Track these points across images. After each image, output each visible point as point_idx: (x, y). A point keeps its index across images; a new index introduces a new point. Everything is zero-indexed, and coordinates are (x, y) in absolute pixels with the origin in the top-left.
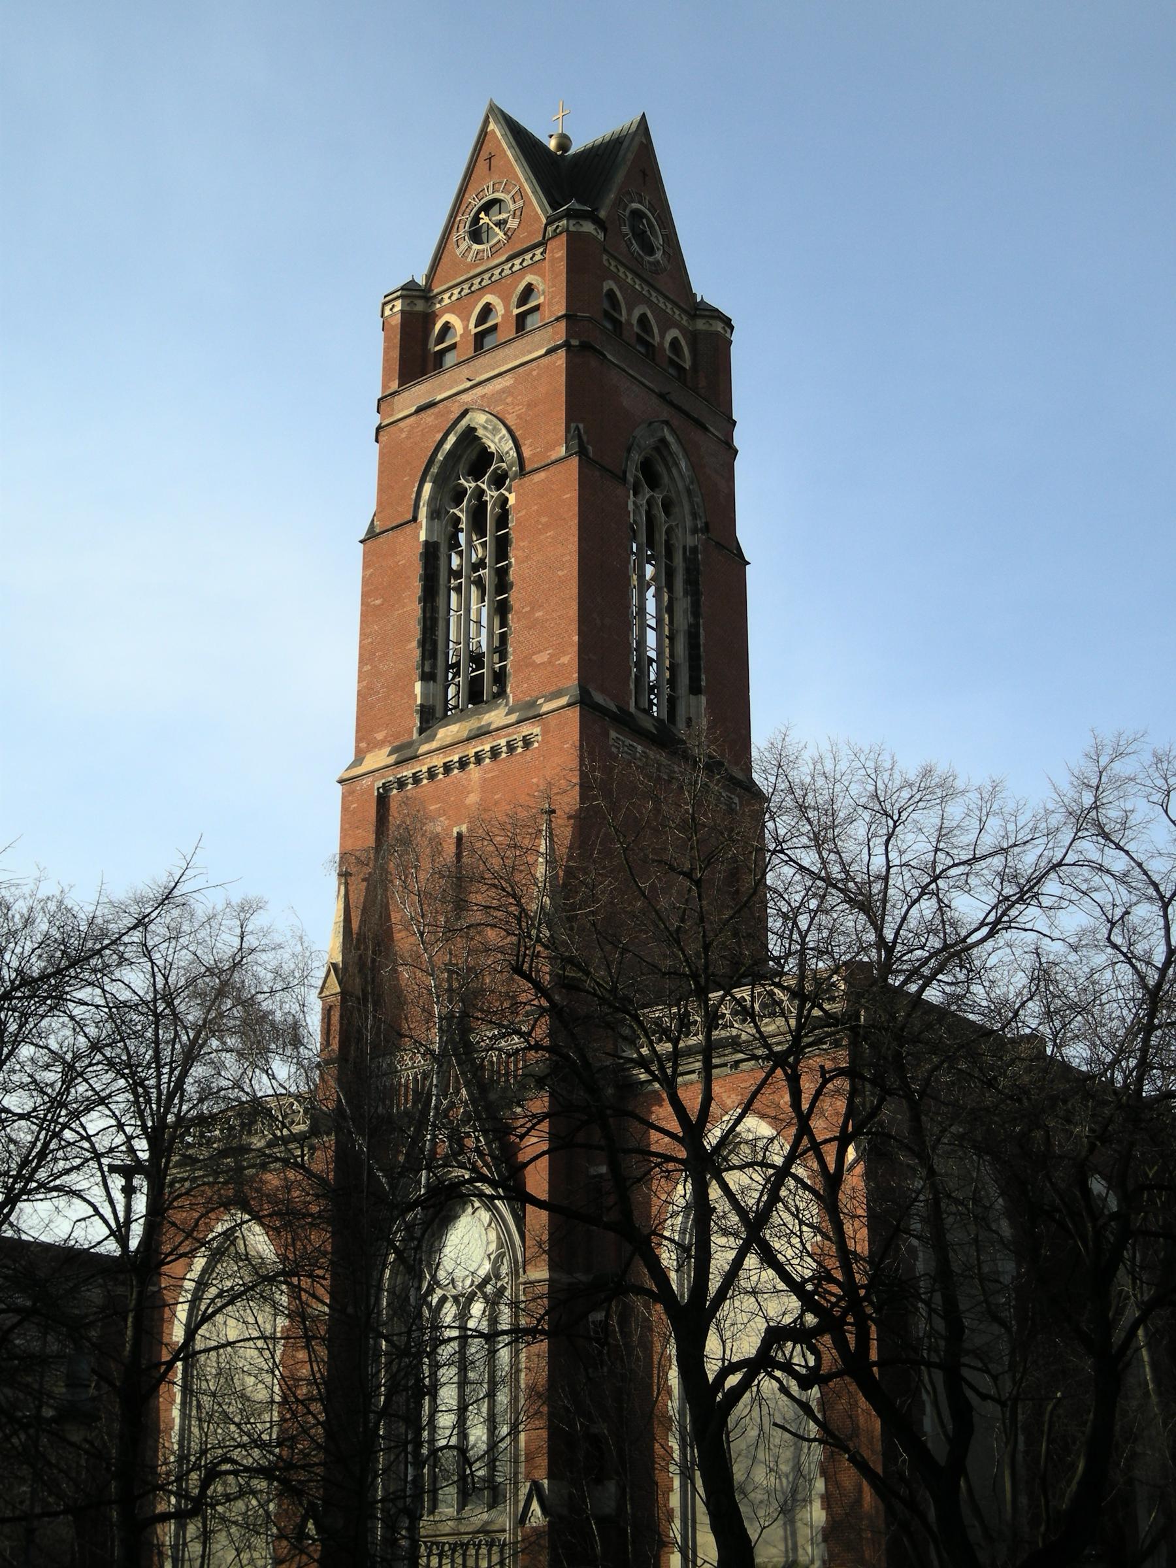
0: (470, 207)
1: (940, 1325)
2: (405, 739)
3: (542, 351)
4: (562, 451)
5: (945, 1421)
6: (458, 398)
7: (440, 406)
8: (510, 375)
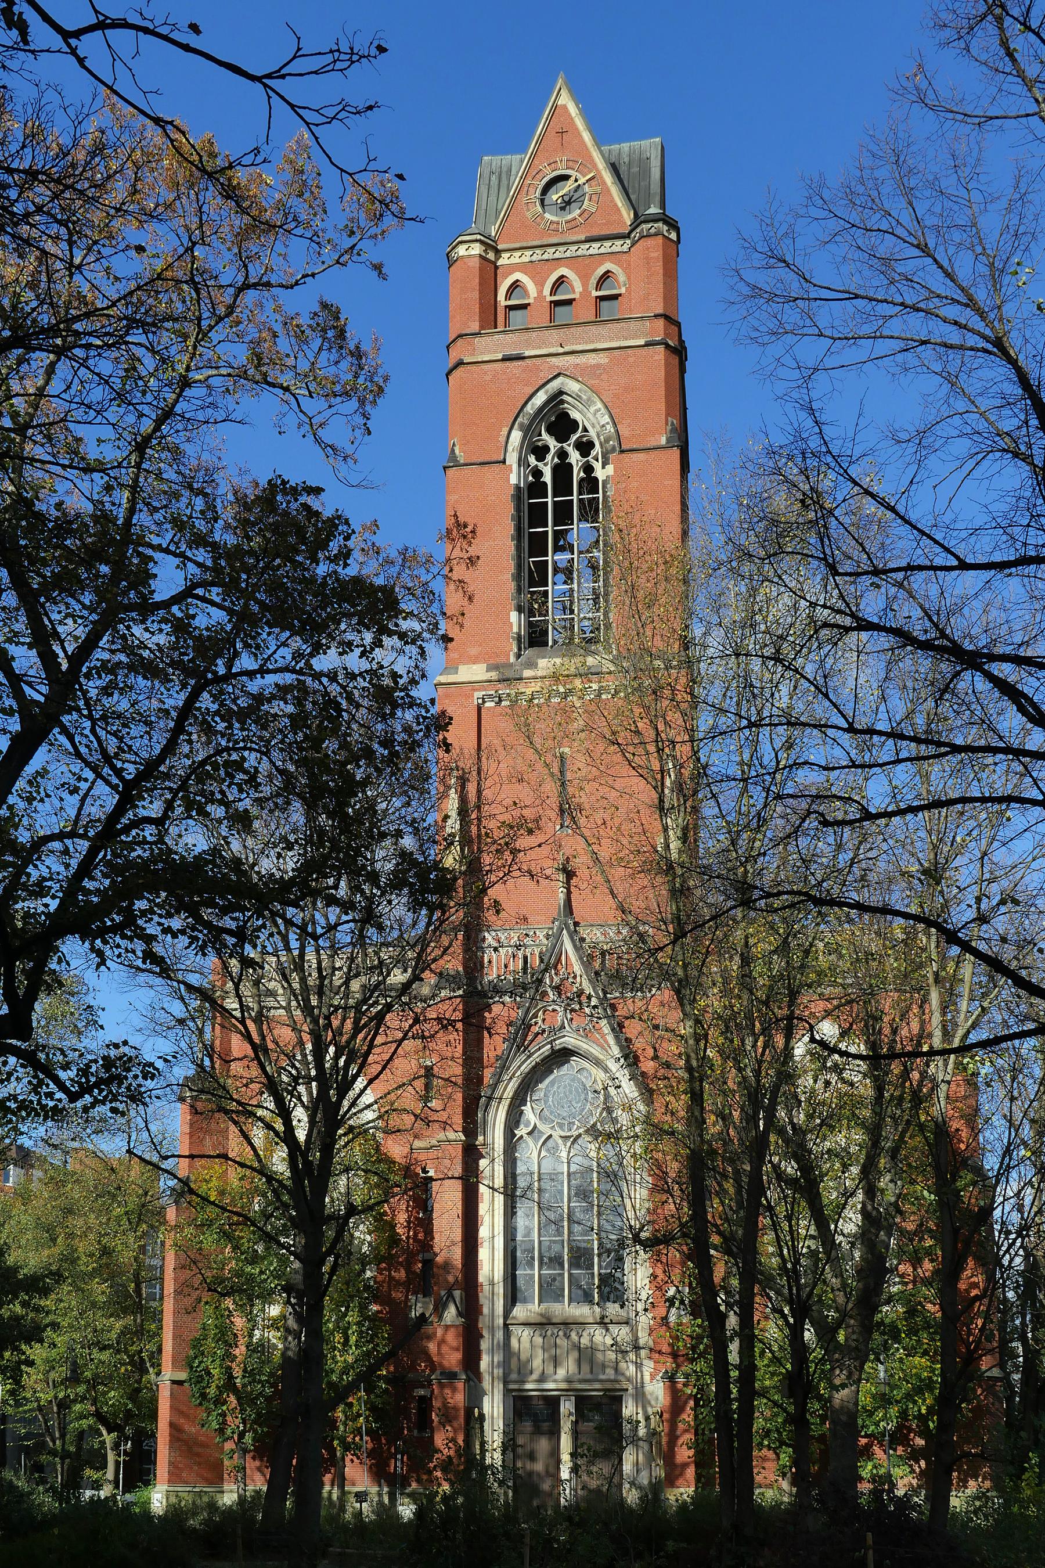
0: (541, 175)
1: (712, 1184)
2: (502, 660)
3: (642, 342)
4: (663, 441)
5: (483, 1232)
6: (548, 359)
7: (528, 361)
8: (607, 353)
